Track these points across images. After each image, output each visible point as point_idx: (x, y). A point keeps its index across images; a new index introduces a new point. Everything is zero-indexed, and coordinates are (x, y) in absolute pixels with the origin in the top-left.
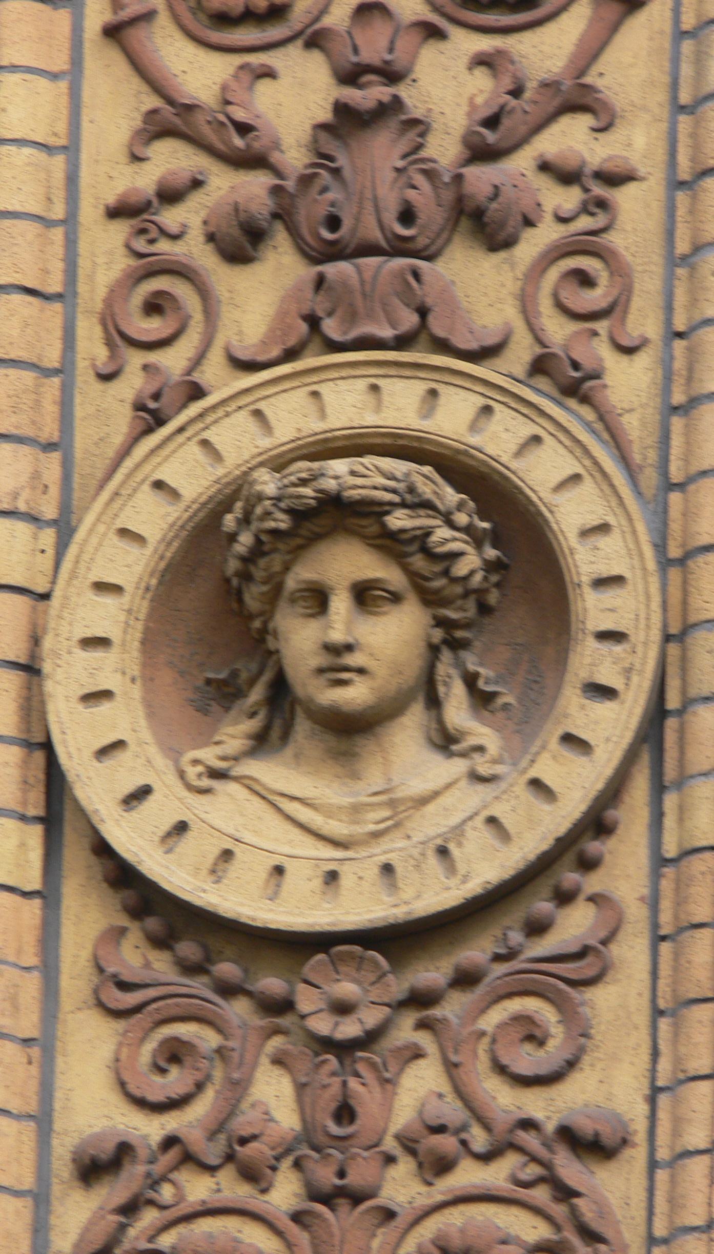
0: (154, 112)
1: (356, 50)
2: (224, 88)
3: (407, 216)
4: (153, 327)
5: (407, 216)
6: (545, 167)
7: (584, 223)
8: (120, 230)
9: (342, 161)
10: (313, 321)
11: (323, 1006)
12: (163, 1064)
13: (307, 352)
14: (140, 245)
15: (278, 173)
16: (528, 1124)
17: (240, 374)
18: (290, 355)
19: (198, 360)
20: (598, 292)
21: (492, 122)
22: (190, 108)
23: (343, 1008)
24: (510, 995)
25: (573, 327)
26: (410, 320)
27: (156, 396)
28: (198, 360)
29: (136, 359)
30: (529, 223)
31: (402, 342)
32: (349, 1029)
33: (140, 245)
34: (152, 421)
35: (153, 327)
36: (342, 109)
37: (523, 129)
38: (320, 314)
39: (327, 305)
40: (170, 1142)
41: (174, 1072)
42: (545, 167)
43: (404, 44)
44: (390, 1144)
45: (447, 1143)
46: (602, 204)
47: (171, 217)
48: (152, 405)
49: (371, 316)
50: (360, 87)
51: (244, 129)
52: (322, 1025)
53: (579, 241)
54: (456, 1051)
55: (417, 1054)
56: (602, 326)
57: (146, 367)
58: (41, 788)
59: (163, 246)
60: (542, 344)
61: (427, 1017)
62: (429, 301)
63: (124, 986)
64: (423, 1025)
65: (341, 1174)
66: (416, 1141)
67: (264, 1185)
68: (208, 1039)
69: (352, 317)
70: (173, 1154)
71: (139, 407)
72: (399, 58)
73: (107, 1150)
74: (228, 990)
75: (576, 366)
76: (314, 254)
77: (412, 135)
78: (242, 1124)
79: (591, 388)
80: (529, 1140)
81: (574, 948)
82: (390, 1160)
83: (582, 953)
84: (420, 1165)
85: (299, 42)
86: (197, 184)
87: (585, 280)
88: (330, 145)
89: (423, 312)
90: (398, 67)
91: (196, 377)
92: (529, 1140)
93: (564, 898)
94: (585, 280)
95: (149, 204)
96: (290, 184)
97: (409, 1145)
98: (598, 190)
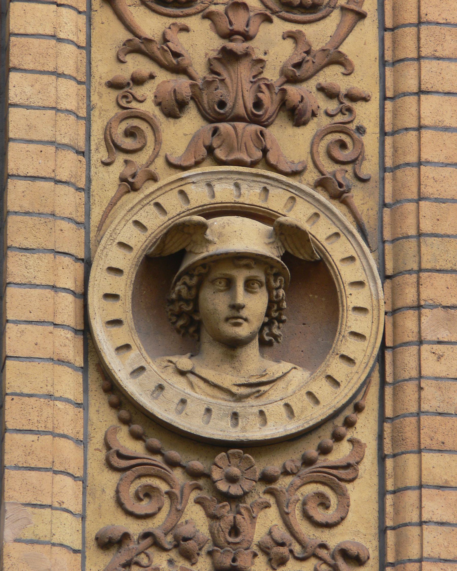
0: (129, 41)
1: (231, 23)
2: (164, 35)
3: (258, 104)
4: (128, 143)
5: (258, 104)
6: (321, 89)
7: (339, 118)
8: (114, 94)
9: (225, 75)
10: (210, 150)
11: (223, 477)
12: (142, 496)
13: (204, 164)
14: (123, 103)
15: (191, 77)
16: (323, 546)
17: (173, 171)
18: (197, 164)
19: (151, 161)
20: (347, 152)
21: (298, 65)
22: (148, 41)
23: (232, 479)
24: (316, 482)
25: (337, 167)
26: (258, 154)
27: (134, 176)
28: (151, 161)
29: (121, 158)
30: (314, 115)
31: (253, 164)
32: (235, 490)
33: (123, 103)
34: (130, 189)
35: (128, 143)
36: (224, 50)
37: (312, 70)
38: (215, 145)
39: (219, 143)
40: (146, 535)
41: (145, 502)
42: (321, 89)
43: (255, 22)
44: (255, 548)
45: (284, 550)
46: (350, 110)
47: (139, 91)
48: (130, 180)
49: (239, 149)
50: (231, 41)
51: (176, 55)
52: (223, 486)
53: (339, 127)
54: (287, 507)
55: (268, 506)
56: (349, 168)
57: (126, 162)
58: (82, 355)
59: (134, 104)
60: (323, 174)
61: (271, 488)
62: (268, 147)
63: (120, 456)
64: (271, 492)
65: (234, 560)
66: (268, 548)
67: (193, 561)
68: (164, 487)
69: (231, 150)
70: (148, 541)
71: (123, 180)
72: (251, 30)
73: (117, 535)
74: (173, 464)
75: (341, 185)
76: (210, 118)
77: (259, 66)
78: (185, 530)
79: (347, 197)
80: (323, 553)
81: (344, 464)
82: (255, 555)
83: (348, 466)
84: (270, 560)
85: (200, 15)
86: (152, 77)
87: (343, 145)
88: (219, 68)
89: (265, 151)
90: (251, 33)
91: (152, 168)
92: (323, 553)
93: (338, 438)
94: (343, 145)
95: (128, 84)
96: (200, 82)
97: (265, 550)
98: (347, 103)
